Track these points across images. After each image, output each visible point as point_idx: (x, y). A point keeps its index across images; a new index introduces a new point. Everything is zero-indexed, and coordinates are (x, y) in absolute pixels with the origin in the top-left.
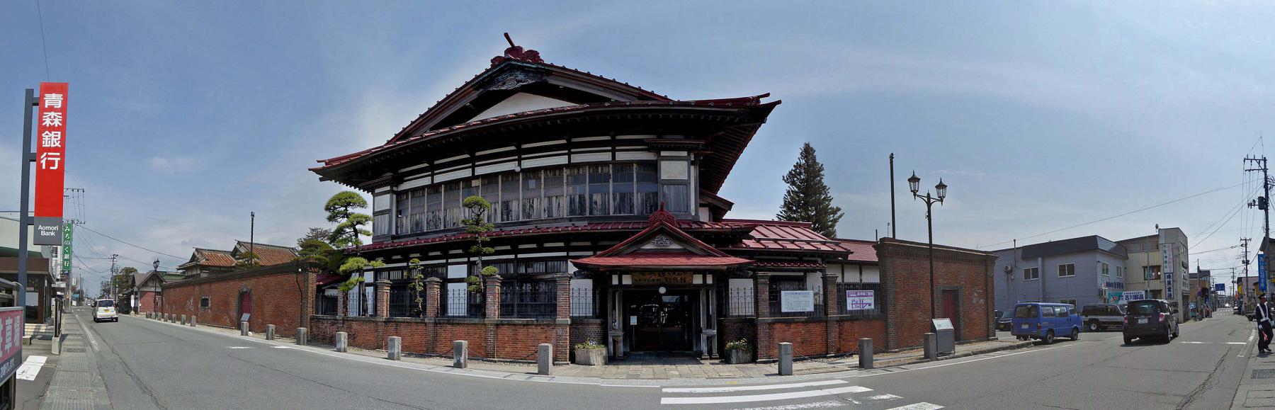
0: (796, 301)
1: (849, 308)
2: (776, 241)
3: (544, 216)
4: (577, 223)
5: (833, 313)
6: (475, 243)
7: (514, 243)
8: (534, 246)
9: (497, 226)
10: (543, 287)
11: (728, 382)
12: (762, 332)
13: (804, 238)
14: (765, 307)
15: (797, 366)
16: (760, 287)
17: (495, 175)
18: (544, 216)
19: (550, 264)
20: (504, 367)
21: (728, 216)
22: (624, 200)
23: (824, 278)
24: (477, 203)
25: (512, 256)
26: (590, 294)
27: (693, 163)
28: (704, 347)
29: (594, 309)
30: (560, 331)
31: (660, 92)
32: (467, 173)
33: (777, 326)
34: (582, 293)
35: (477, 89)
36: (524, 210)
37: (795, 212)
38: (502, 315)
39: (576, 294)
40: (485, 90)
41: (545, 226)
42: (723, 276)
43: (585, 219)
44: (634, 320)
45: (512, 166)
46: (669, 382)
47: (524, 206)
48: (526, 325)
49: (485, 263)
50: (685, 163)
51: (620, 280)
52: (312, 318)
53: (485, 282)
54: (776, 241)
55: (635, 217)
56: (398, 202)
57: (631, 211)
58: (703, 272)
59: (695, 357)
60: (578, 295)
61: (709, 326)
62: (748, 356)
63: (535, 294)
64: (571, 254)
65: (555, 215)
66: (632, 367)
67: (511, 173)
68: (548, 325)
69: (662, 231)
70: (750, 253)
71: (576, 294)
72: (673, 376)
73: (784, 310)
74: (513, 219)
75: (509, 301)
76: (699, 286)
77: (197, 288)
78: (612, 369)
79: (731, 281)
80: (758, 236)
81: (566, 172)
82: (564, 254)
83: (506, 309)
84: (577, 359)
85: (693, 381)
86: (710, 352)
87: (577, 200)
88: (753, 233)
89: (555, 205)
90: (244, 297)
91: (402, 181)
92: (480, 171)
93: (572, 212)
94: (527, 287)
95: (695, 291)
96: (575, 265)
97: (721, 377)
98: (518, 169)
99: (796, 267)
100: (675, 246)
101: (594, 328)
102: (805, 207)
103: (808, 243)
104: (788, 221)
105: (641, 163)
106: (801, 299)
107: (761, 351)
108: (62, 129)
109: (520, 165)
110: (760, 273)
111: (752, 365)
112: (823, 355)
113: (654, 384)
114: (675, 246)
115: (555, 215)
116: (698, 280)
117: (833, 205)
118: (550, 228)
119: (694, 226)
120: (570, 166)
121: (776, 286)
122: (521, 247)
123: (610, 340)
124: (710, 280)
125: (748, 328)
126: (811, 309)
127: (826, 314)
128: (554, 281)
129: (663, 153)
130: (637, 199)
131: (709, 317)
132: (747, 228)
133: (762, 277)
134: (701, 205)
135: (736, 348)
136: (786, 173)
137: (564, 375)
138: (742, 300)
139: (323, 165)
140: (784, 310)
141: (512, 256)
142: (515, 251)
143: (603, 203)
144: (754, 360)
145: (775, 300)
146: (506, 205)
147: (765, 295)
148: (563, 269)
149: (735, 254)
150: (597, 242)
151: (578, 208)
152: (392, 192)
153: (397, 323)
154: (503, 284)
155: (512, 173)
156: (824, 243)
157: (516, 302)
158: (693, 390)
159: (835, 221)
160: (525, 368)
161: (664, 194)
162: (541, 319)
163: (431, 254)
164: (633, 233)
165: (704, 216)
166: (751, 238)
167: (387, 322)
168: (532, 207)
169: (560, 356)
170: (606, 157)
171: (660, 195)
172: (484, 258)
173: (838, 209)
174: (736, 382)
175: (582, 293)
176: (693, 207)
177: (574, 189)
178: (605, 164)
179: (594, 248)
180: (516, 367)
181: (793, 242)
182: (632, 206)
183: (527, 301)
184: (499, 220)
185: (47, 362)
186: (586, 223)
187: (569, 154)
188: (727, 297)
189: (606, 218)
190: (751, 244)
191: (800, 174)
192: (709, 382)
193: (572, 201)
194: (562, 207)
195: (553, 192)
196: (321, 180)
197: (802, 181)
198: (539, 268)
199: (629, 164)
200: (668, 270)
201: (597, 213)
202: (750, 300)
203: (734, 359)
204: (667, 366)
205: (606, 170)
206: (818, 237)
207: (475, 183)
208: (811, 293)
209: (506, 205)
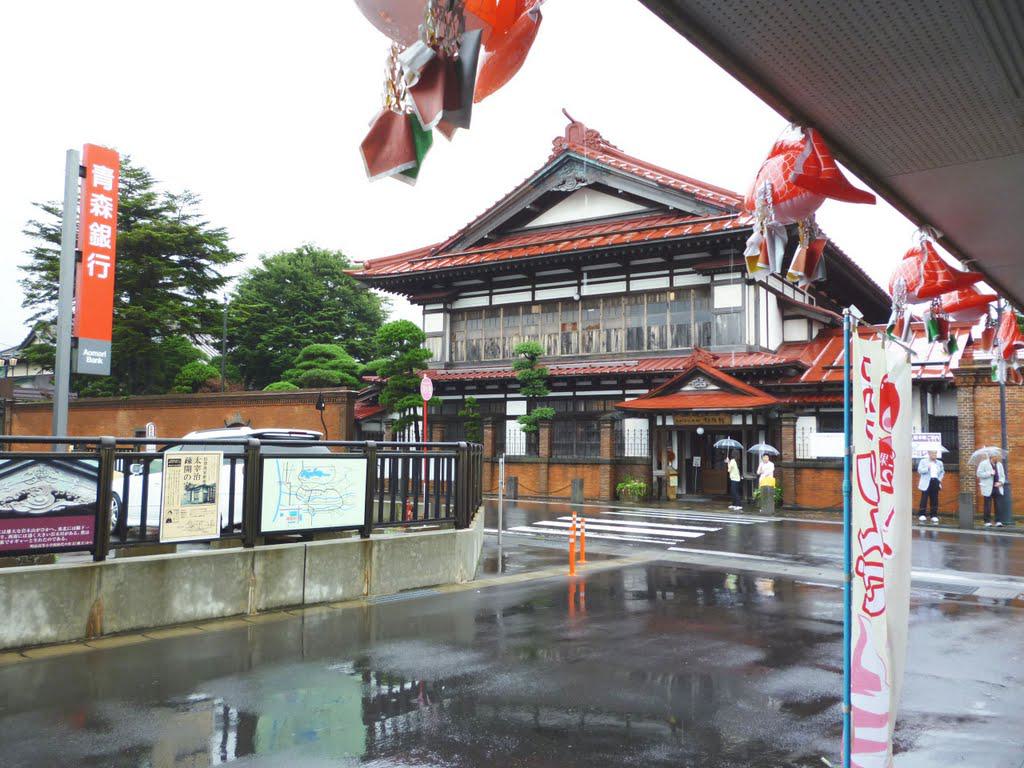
32: (526, 297)
40: (542, 193)
45: (570, 292)
47: (584, 338)
50: (739, 287)
51: (664, 421)
57: (688, 344)
64: (628, 392)
65: (613, 350)
91: (457, 298)
92: (541, 295)
93: (629, 346)
98: (576, 297)
108: (89, 218)
109: (579, 290)
120: (628, 294)
141: (571, 394)
143: (661, 335)
161: (717, 324)
163: (489, 387)
168: (591, 339)
171: (714, 327)
175: (638, 434)
182: (689, 337)
184: (558, 353)
187: (671, 276)
198: (596, 407)
199: (687, 289)
201: (655, 348)
207: (535, 309)
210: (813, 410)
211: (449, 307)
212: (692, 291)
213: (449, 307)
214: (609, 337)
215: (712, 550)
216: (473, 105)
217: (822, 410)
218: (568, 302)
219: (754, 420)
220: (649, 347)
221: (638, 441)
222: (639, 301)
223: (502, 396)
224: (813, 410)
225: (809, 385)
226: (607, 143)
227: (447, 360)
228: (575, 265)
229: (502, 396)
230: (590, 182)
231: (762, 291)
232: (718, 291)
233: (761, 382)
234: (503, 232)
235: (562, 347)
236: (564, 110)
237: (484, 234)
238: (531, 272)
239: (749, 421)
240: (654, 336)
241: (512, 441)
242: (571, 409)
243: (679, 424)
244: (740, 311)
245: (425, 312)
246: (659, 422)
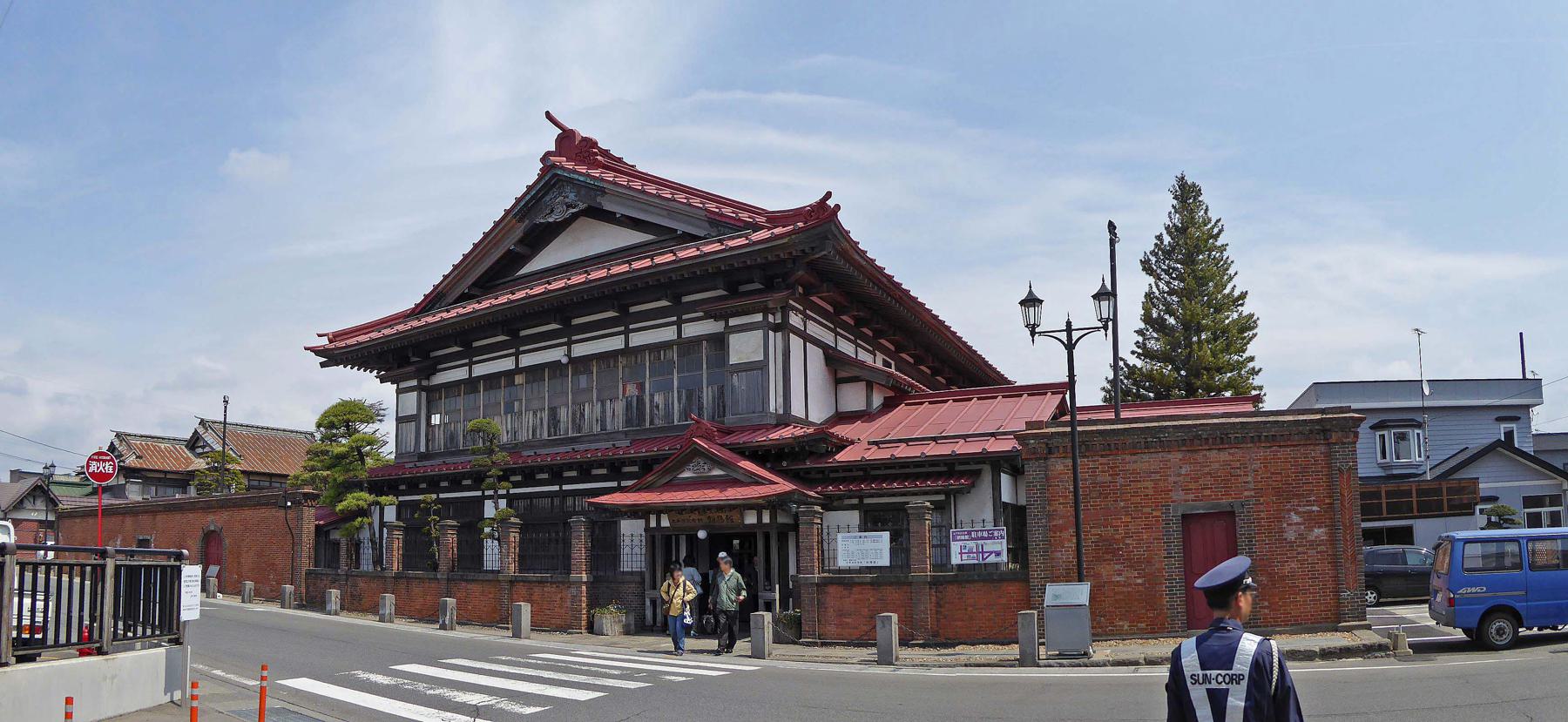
1: (956, 560)
3: (597, 429)
5: (924, 569)
18: (597, 429)
25: (556, 488)
30: (573, 590)
31: (468, 248)
32: (507, 364)
33: (832, 590)
35: (521, 220)
40: (530, 223)
45: (557, 354)
47: (574, 414)
48: (541, 582)
52: (309, 573)
56: (428, 402)
58: (757, 506)
67: (555, 365)
71: (627, 541)
77: (129, 521)
81: (622, 361)
89: (609, 414)
90: (210, 538)
91: (434, 371)
92: (527, 360)
93: (628, 422)
98: (565, 360)
100: (717, 472)
109: (569, 350)
114: (717, 472)
116: (751, 519)
120: (627, 351)
129: (733, 322)
139: (324, 341)
141: (556, 488)
146: (553, 412)
151: (635, 412)
152: (419, 388)
153: (409, 579)
167: (397, 577)
168: (582, 415)
170: (669, 334)
182: (700, 408)
193: (628, 406)
196: (323, 365)
199: (697, 341)
201: (659, 423)
209: (553, 412)
210: (855, 501)
211: (424, 383)
213: (424, 383)
214: (603, 411)
215: (242, 676)
216: (1267, 406)
217: (867, 501)
219: (773, 517)
223: (479, 493)
224: (855, 501)
225: (849, 467)
226: (606, 153)
227: (423, 449)
228: (564, 312)
229: (479, 493)
230: (582, 206)
231: (796, 343)
232: (735, 340)
233: (785, 464)
234: (488, 282)
236: (548, 114)
237: (463, 287)
238: (512, 327)
239: (766, 519)
241: (627, 550)
244: (762, 366)
245: (399, 392)
246: (653, 524)
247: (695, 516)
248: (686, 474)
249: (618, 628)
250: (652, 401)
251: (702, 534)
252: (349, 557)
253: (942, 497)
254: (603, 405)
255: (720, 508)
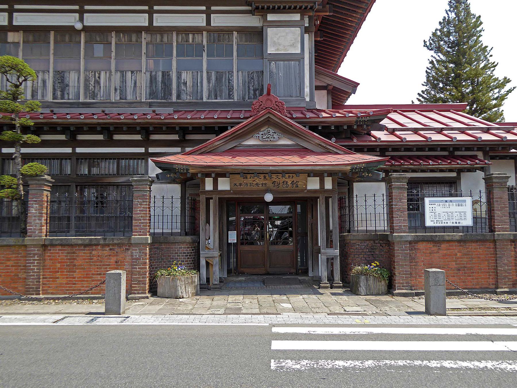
0: (445, 212)
2: (415, 131)
4: (159, 110)
6: (12, 127)
7: (72, 132)
8: (100, 137)
9: (46, 105)
10: (113, 195)
11: (357, 319)
12: (400, 254)
13: (455, 125)
14: (402, 219)
15: (451, 303)
16: (395, 192)
17: (45, 30)
18: (115, 97)
19: (123, 162)
20: (54, 307)
21: (352, 100)
22: (221, 79)
23: (489, 181)
24: (14, 67)
25: (69, 150)
26: (178, 204)
27: (307, 30)
28: (323, 272)
29: (183, 223)
30: (136, 253)
33: (421, 246)
34: (168, 202)
36: (86, 87)
37: (442, 90)
38: (51, 232)
39: (159, 204)
41: (115, 111)
42: (346, 180)
43: (171, 104)
44: (233, 237)
45: (69, 20)
46: (279, 319)
47: (87, 80)
49: (27, 158)
53: (26, 185)
54: (415, 131)
55: (234, 104)
57: (230, 96)
58: (320, 174)
59: (313, 285)
60: (161, 205)
61: (330, 244)
62: (383, 285)
63: (101, 203)
64: (151, 150)
65: (130, 97)
66: (231, 298)
68: (119, 245)
69: (268, 122)
70: (382, 149)
72: (284, 310)
73: (429, 223)
74: (71, 98)
75: (62, 213)
76: (315, 191)
78: (205, 300)
79: (356, 186)
80: (392, 125)
82: (142, 150)
83: (58, 223)
84: (160, 290)
85: (309, 318)
86: (331, 279)
87: (160, 78)
88: (385, 122)
89: (130, 84)
93: (152, 94)
94: (90, 194)
95: (308, 202)
96: (158, 164)
97: (347, 313)
98: (79, 26)
99: (444, 165)
100: (285, 142)
101: (183, 247)
102: (457, 80)
103: (462, 131)
104: (429, 104)
105: (241, 30)
106: (454, 208)
107: (398, 279)
109: (81, 19)
110: (395, 175)
111: (388, 298)
112: (491, 290)
113: (261, 321)
114: (285, 142)
115: (130, 97)
116: (313, 184)
117: (499, 74)
118: (124, 113)
119: (309, 115)
121: (416, 192)
122: (80, 137)
123: (203, 262)
124: (328, 185)
125: (381, 245)
126: (468, 222)
127: (492, 230)
128: (129, 185)
129: (271, 17)
130: (237, 80)
131: (329, 233)
132: (377, 115)
133: (398, 179)
134: (318, 88)
135: (365, 274)
136: (427, 36)
137: (144, 315)
138: (370, 210)
140: (429, 223)
141: (69, 150)
142: (73, 142)
143: (195, 84)
144: (390, 289)
145: (416, 208)
146: (60, 79)
147: (402, 203)
148: (141, 170)
149: (360, 150)
150: (185, 135)
151: (160, 88)
154: (55, 188)
155: (71, 29)
156: (487, 131)
157: (74, 213)
158: (312, 330)
159: (502, 98)
160: (86, 307)
161: (271, 72)
162: (109, 237)
164: (233, 125)
165: (322, 101)
166: (383, 128)
168: (97, 82)
169: (136, 287)
171: (266, 75)
172: (24, 150)
173: (507, 81)
174: (368, 320)
175: (168, 202)
176: (307, 90)
177: (156, 63)
178: (197, 30)
179: (182, 143)
180: (74, 306)
181: (440, 131)
182: (231, 89)
183: (90, 211)
184: (49, 98)
185: (506, 182)
186: (170, 110)
187: (151, 13)
188: (351, 207)
189: (198, 105)
190: (382, 136)
191: (449, 34)
192: (331, 319)
193: (153, 80)
194: (139, 86)
195: (126, 66)
197: (453, 45)
198: (108, 168)
199: (228, 31)
200: (276, 172)
201: (186, 98)
202: (382, 209)
203: (362, 289)
204: (276, 297)
205: (198, 38)
206: (478, 122)
208: (469, 200)
209: (60, 79)
212: (52, 33)
214: (123, 81)
218: (65, 32)
220: (178, 97)
221: (168, 212)
222: (134, 38)
232: (271, 33)
235: (54, 90)
240: (185, 84)
242: (68, 170)
243: (239, 188)
247: (260, 180)
248: (251, 142)
249: (191, 290)
250: (179, 77)
251: (269, 197)
252: (170, 80)
253: (454, 174)
254: (123, 74)
255: (284, 173)
